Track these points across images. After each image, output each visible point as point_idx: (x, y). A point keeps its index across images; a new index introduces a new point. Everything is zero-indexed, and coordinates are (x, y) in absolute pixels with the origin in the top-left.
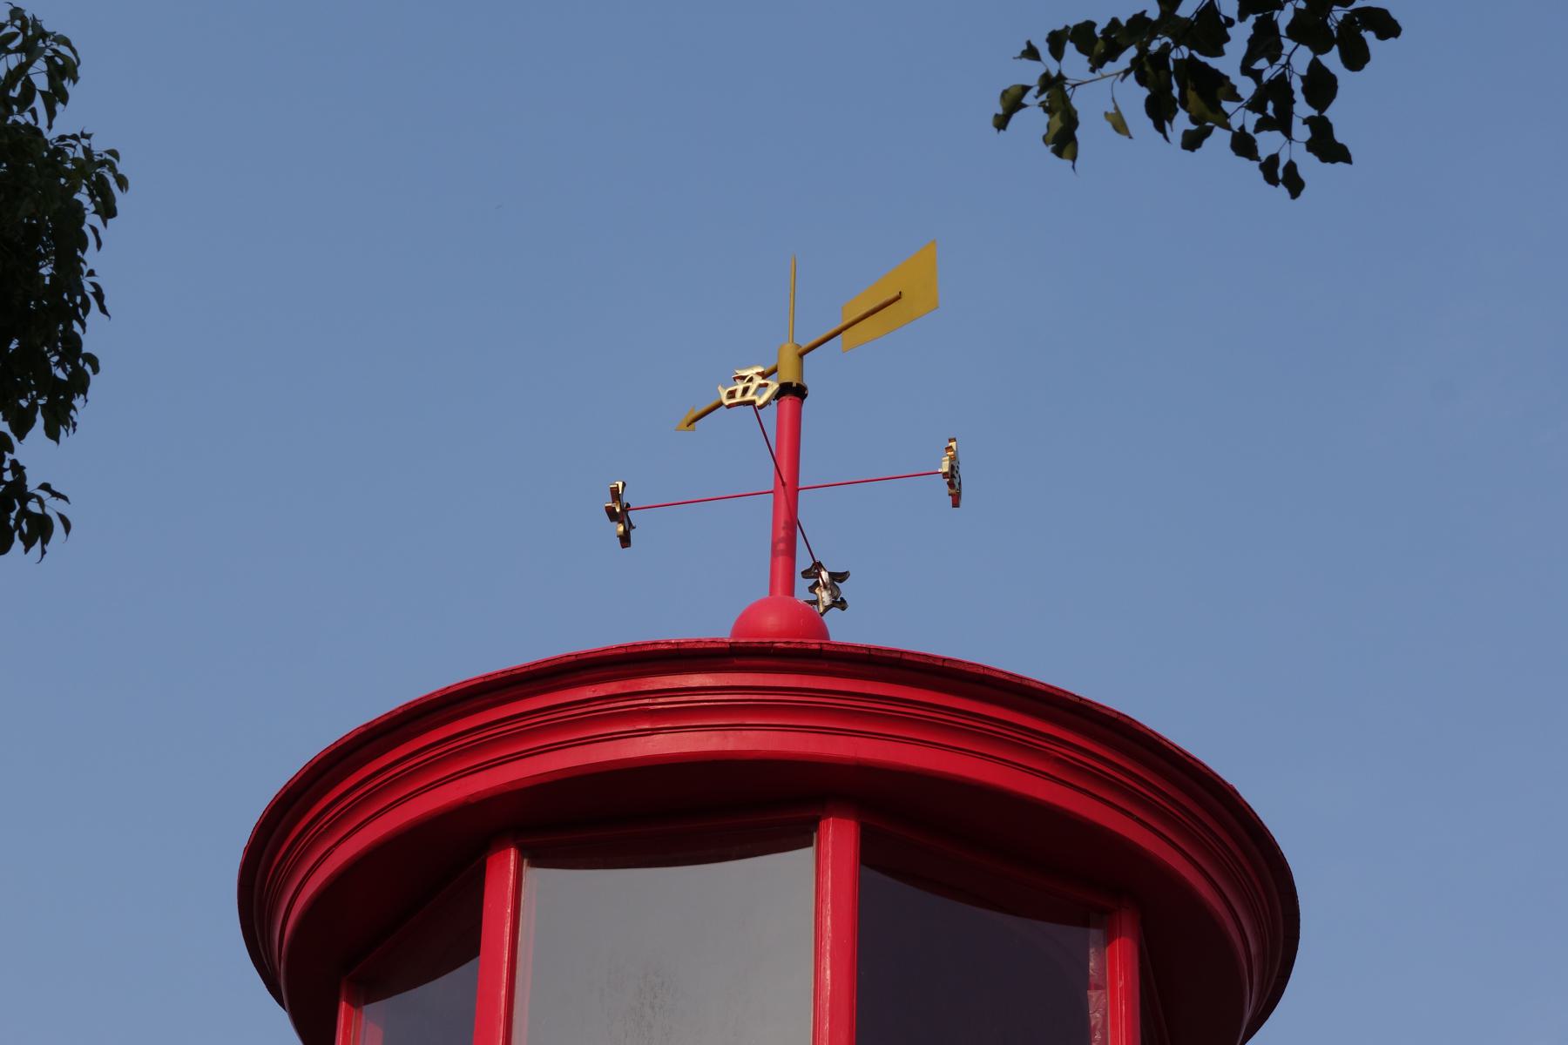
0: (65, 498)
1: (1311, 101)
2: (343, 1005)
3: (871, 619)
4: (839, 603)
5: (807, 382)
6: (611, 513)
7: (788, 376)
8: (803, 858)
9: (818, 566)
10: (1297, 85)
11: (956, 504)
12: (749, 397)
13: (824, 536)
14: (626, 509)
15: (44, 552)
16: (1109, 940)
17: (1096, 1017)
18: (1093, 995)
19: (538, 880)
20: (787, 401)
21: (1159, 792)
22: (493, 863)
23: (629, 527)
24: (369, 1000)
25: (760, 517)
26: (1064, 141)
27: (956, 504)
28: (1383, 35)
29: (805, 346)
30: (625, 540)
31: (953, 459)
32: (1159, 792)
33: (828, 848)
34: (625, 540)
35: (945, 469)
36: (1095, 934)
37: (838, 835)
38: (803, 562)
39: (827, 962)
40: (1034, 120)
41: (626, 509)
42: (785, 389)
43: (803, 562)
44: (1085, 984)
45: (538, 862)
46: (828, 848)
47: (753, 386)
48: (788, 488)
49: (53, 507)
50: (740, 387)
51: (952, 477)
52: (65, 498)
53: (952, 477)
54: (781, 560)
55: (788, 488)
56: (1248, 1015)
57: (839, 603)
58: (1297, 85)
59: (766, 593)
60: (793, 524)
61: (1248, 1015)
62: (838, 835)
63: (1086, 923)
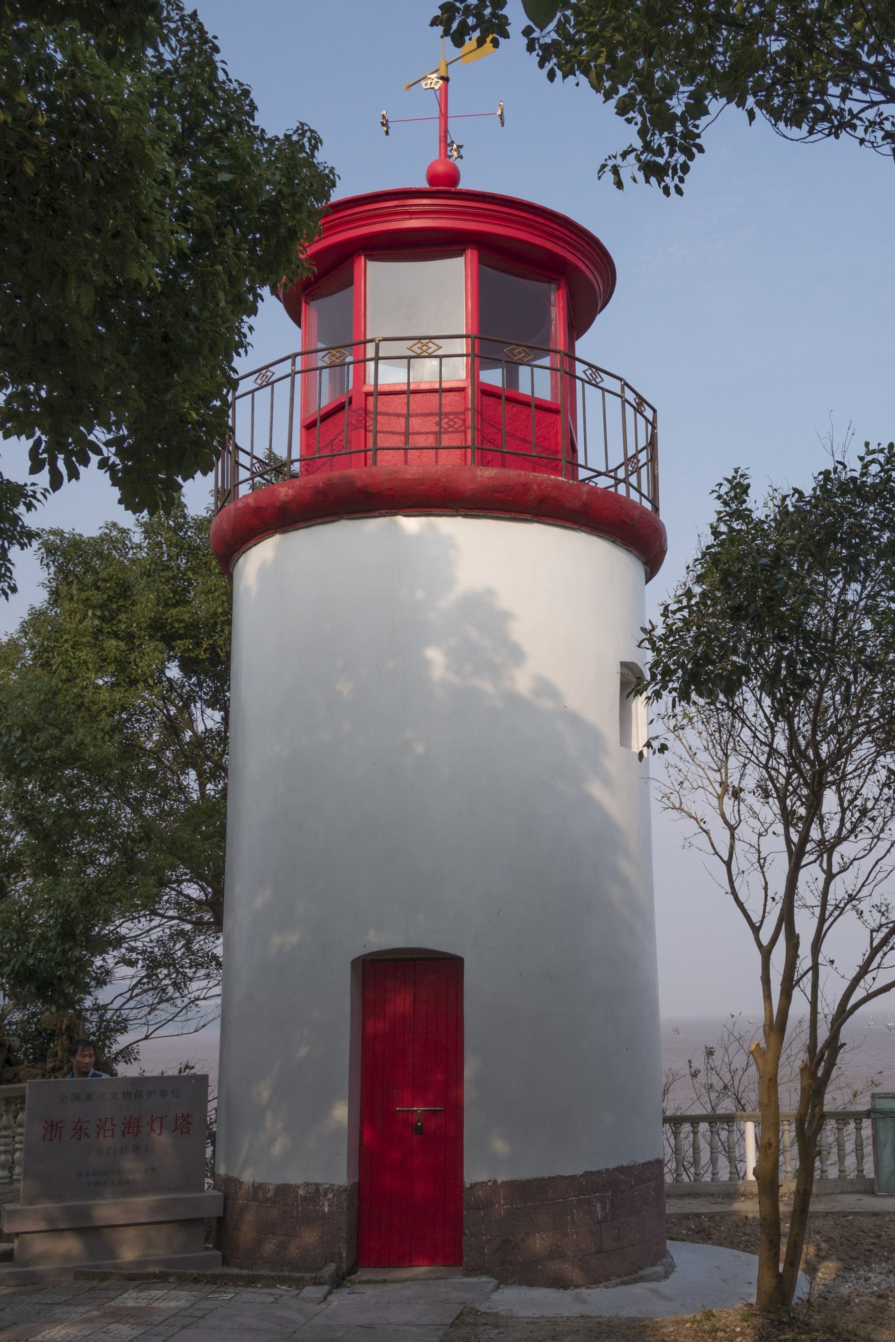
1: (682, 171)
4: (461, 157)
5: (449, 76)
6: (383, 124)
7: (443, 74)
9: (453, 142)
10: (678, 166)
11: (503, 125)
12: (432, 86)
13: (456, 134)
14: (387, 121)
16: (559, 289)
17: (553, 316)
18: (553, 308)
19: (369, 263)
23: (388, 128)
25: (435, 125)
26: (619, 184)
27: (503, 125)
28: (699, 152)
29: (449, 61)
30: (387, 133)
31: (502, 109)
34: (387, 133)
35: (499, 113)
36: (553, 286)
37: (471, 254)
38: (449, 142)
40: (609, 176)
44: (550, 304)
45: (370, 260)
47: (434, 82)
48: (444, 116)
50: (429, 81)
51: (501, 116)
53: (501, 116)
55: (444, 116)
56: (599, 307)
57: (461, 157)
58: (678, 166)
60: (446, 131)
61: (599, 307)
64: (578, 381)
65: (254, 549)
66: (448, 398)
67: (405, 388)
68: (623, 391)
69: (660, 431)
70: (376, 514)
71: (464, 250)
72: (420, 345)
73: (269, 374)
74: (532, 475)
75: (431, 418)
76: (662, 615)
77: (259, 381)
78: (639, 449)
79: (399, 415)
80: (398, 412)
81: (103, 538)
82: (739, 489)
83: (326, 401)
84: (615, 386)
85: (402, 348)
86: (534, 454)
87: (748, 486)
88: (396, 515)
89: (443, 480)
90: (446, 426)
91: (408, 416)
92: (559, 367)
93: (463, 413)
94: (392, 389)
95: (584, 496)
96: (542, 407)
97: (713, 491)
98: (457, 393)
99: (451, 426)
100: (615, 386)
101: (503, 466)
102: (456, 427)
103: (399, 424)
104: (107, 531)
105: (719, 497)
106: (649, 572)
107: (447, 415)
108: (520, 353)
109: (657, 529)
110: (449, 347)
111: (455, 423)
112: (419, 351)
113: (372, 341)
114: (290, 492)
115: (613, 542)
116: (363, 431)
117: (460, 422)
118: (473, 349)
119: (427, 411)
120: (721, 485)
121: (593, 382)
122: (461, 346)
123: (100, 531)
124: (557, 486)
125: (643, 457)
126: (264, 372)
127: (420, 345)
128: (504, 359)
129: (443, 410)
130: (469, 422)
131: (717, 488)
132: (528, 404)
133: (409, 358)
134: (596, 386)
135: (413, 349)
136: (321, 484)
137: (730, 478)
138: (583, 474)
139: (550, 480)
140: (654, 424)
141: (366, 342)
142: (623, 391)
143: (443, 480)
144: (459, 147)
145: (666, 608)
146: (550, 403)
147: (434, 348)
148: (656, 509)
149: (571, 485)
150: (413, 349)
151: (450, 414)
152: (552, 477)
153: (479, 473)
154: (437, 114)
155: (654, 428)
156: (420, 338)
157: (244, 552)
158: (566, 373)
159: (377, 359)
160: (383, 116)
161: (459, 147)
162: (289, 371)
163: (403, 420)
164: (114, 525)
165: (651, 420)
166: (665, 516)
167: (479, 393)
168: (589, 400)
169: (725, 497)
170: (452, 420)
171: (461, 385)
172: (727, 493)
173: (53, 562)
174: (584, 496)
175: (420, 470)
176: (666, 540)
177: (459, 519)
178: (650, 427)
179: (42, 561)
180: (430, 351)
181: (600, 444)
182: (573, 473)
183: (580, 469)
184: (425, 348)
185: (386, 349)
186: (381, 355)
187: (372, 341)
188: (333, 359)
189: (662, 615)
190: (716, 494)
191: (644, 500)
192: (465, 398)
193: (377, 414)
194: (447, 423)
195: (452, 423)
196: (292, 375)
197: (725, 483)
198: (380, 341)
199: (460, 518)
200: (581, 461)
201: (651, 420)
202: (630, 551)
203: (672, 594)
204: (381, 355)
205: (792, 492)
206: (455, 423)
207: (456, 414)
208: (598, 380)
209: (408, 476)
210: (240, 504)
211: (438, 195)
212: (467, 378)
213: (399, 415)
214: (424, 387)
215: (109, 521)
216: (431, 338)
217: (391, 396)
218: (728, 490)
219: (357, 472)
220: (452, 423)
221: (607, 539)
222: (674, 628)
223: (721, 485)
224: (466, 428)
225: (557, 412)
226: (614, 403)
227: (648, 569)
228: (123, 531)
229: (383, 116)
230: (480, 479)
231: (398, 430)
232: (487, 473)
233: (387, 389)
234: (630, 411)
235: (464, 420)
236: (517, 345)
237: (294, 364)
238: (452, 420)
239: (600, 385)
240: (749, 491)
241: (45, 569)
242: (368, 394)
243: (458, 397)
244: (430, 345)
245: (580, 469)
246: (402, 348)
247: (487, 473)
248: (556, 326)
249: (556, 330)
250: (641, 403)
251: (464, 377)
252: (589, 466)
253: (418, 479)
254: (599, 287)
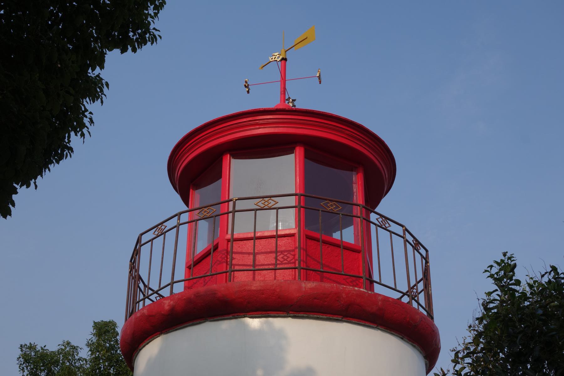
0: (159, 31)
2: (191, 190)
3: (303, 103)
6: (245, 85)
8: (292, 156)
9: (289, 98)
11: (320, 83)
13: (291, 93)
14: (248, 85)
15: (105, 96)
16: (357, 174)
17: (355, 190)
18: (354, 185)
19: (233, 161)
20: (283, 61)
21: (362, 138)
22: (224, 157)
24: (196, 189)
25: (278, 86)
27: (320, 83)
30: (248, 92)
32: (362, 138)
33: (298, 153)
34: (248, 92)
36: (354, 173)
37: (299, 151)
38: (287, 97)
39: (298, 178)
41: (248, 85)
42: (283, 59)
43: (287, 97)
44: (352, 183)
46: (298, 153)
48: (284, 80)
49: (156, 33)
51: (319, 77)
52: (159, 31)
53: (319, 77)
54: (283, 95)
55: (284, 80)
56: (385, 189)
59: (279, 103)
60: (285, 89)
61: (385, 189)
62: (299, 151)
63: (352, 171)
64: (373, 227)
65: (147, 346)
66: (282, 242)
67: (252, 235)
68: (404, 234)
69: (431, 264)
70: (231, 316)
71: (294, 148)
72: (263, 202)
73: (163, 227)
74: (341, 287)
75: (271, 254)
76: (453, 361)
77: (156, 233)
78: (418, 280)
79: (249, 254)
80: (249, 251)
81: (59, 352)
82: (507, 268)
83: (202, 246)
84: (400, 230)
85: (251, 204)
86: (343, 273)
87: (515, 265)
88: (245, 317)
89: (278, 290)
90: (282, 260)
91: (255, 254)
92: (359, 215)
93: (294, 251)
94: (245, 236)
95: (380, 303)
96: (348, 248)
97: (486, 271)
98: (289, 238)
99: (285, 260)
100: (400, 230)
101: (322, 280)
102: (289, 260)
103: (249, 260)
104: (63, 347)
105: (492, 276)
106: (428, 366)
107: (282, 252)
108: (332, 206)
109: (433, 331)
110: (282, 202)
111: (288, 257)
112: (263, 206)
113: (231, 200)
114: (172, 302)
115: (402, 338)
116: (225, 264)
117: (291, 257)
118: (300, 203)
119: (269, 250)
120: (491, 266)
121: (384, 226)
122: (292, 201)
123: (59, 347)
124: (361, 295)
125: (421, 286)
126: (160, 226)
127: (263, 202)
128: (321, 209)
129: (278, 250)
130: (297, 256)
131: (489, 269)
132: (338, 246)
133: (256, 210)
134: (385, 229)
135: (258, 204)
136: (193, 296)
137: (499, 261)
138: (378, 289)
139: (355, 290)
140: (426, 259)
141: (228, 201)
142: (404, 234)
143: (278, 290)
144: (294, 100)
145: (456, 354)
146: (354, 245)
147: (273, 203)
148: (430, 315)
149: (370, 295)
150: (258, 204)
151: (285, 251)
152: (356, 288)
153: (303, 285)
154: (279, 78)
155: (427, 262)
156: (263, 197)
157: (140, 350)
158: (364, 219)
159: (234, 211)
160: (246, 82)
161: (294, 100)
162: (175, 224)
163: (251, 257)
164: (68, 343)
165: (425, 256)
166: (438, 321)
167: (305, 237)
168: (381, 240)
169: (495, 276)
170: (286, 255)
171: (292, 232)
172: (497, 273)
173: (27, 367)
174: (380, 303)
175: (262, 284)
176: (440, 340)
177: (290, 319)
178: (424, 261)
179: (20, 366)
180: (270, 205)
181: (391, 274)
182: (371, 287)
183: (375, 284)
184: (266, 203)
185: (240, 205)
186: (237, 209)
187: (231, 200)
188: (205, 214)
189: (453, 361)
190: (488, 274)
191: (421, 310)
192: (295, 241)
193: (233, 253)
194: (282, 258)
195: (286, 258)
196: (177, 227)
197: (495, 265)
198: (236, 200)
199: (290, 319)
200: (376, 278)
201: (425, 256)
202: (414, 347)
203: (461, 342)
204: (237, 209)
205: (549, 269)
206: (288, 257)
207: (289, 251)
208: (387, 225)
209: (253, 288)
210: (138, 315)
211: (277, 113)
212: (296, 228)
213: (249, 254)
214: (266, 234)
215: (66, 340)
216: (271, 197)
217: (245, 242)
218: (497, 271)
219: (219, 286)
220: (286, 258)
221: (397, 336)
222: (463, 373)
223: (491, 266)
224: (296, 260)
225: (359, 252)
226: (398, 242)
227: (428, 362)
228: (75, 348)
229: (246, 82)
230: (304, 290)
231: (249, 263)
232: (309, 285)
233: (242, 236)
234: (410, 248)
235: (294, 255)
236: (329, 200)
237: (179, 219)
238: (286, 255)
239: (388, 228)
240: (515, 270)
241: (22, 372)
242: (229, 241)
243: (290, 241)
244: (270, 201)
245: (375, 284)
246: (251, 204)
247: (309, 285)
248: (356, 196)
249: (357, 198)
250: (417, 245)
251: (294, 227)
252: (383, 282)
253: (260, 290)
254: (385, 173)
